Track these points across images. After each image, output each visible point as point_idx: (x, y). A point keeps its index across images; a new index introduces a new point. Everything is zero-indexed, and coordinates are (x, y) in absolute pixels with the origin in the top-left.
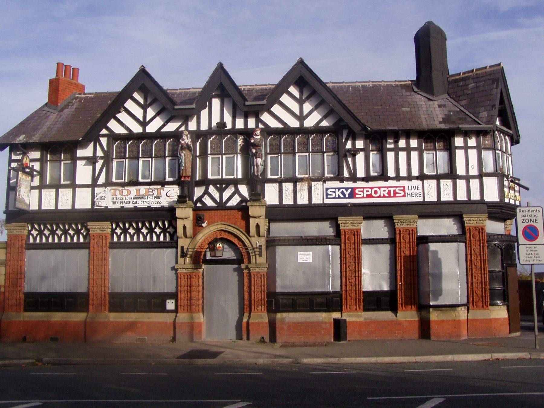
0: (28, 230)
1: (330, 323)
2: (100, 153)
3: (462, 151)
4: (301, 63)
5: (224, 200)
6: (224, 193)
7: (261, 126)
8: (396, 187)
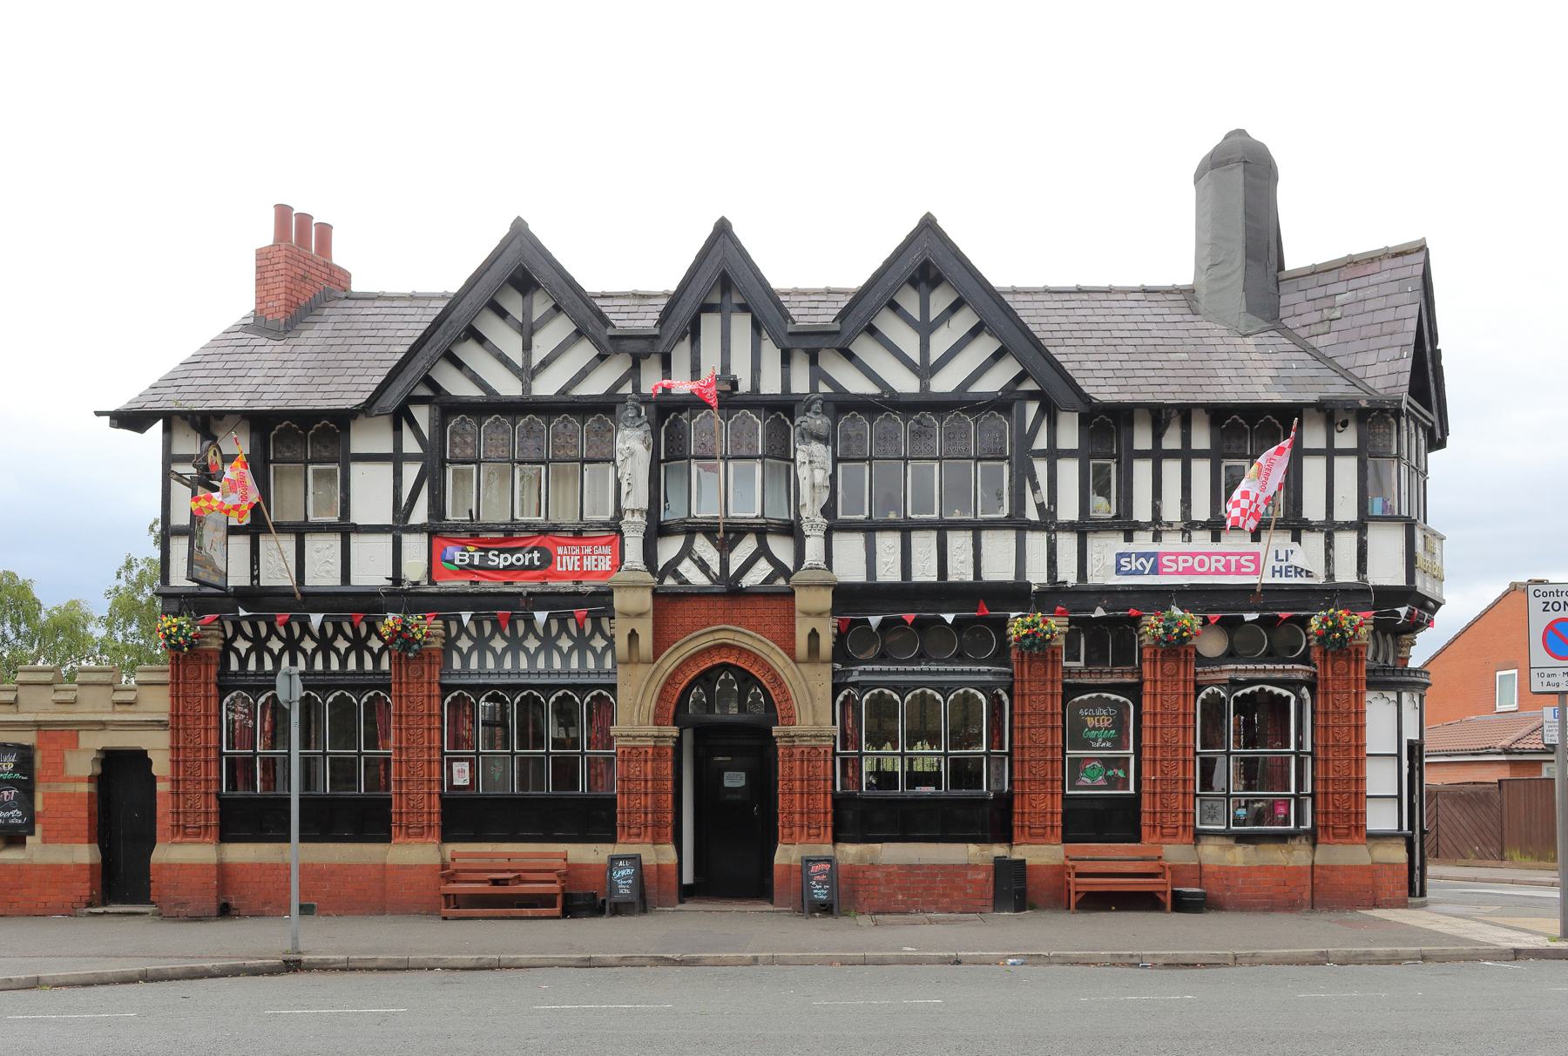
0: (225, 639)
1: (985, 868)
2: (411, 445)
3: (1321, 463)
4: (928, 225)
5: (733, 570)
6: (732, 556)
7: (824, 388)
8: (1242, 555)
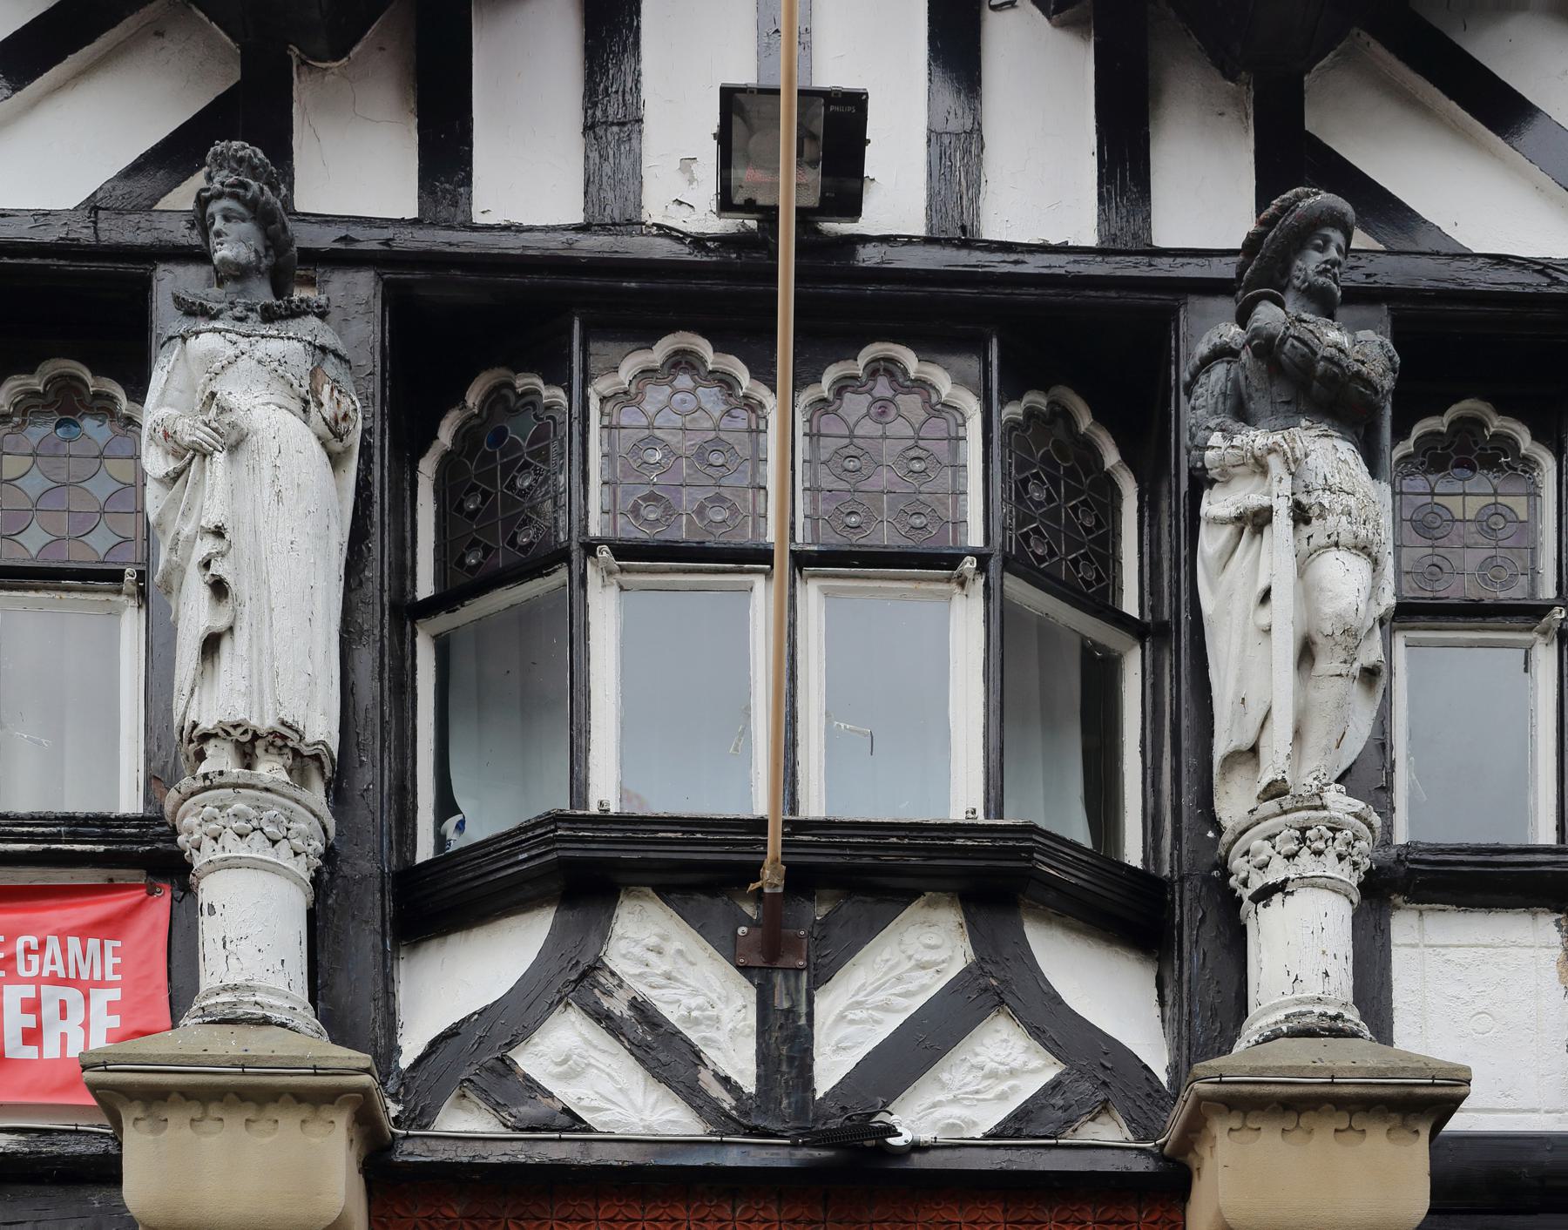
5: (831, 1068)
6: (830, 1005)
